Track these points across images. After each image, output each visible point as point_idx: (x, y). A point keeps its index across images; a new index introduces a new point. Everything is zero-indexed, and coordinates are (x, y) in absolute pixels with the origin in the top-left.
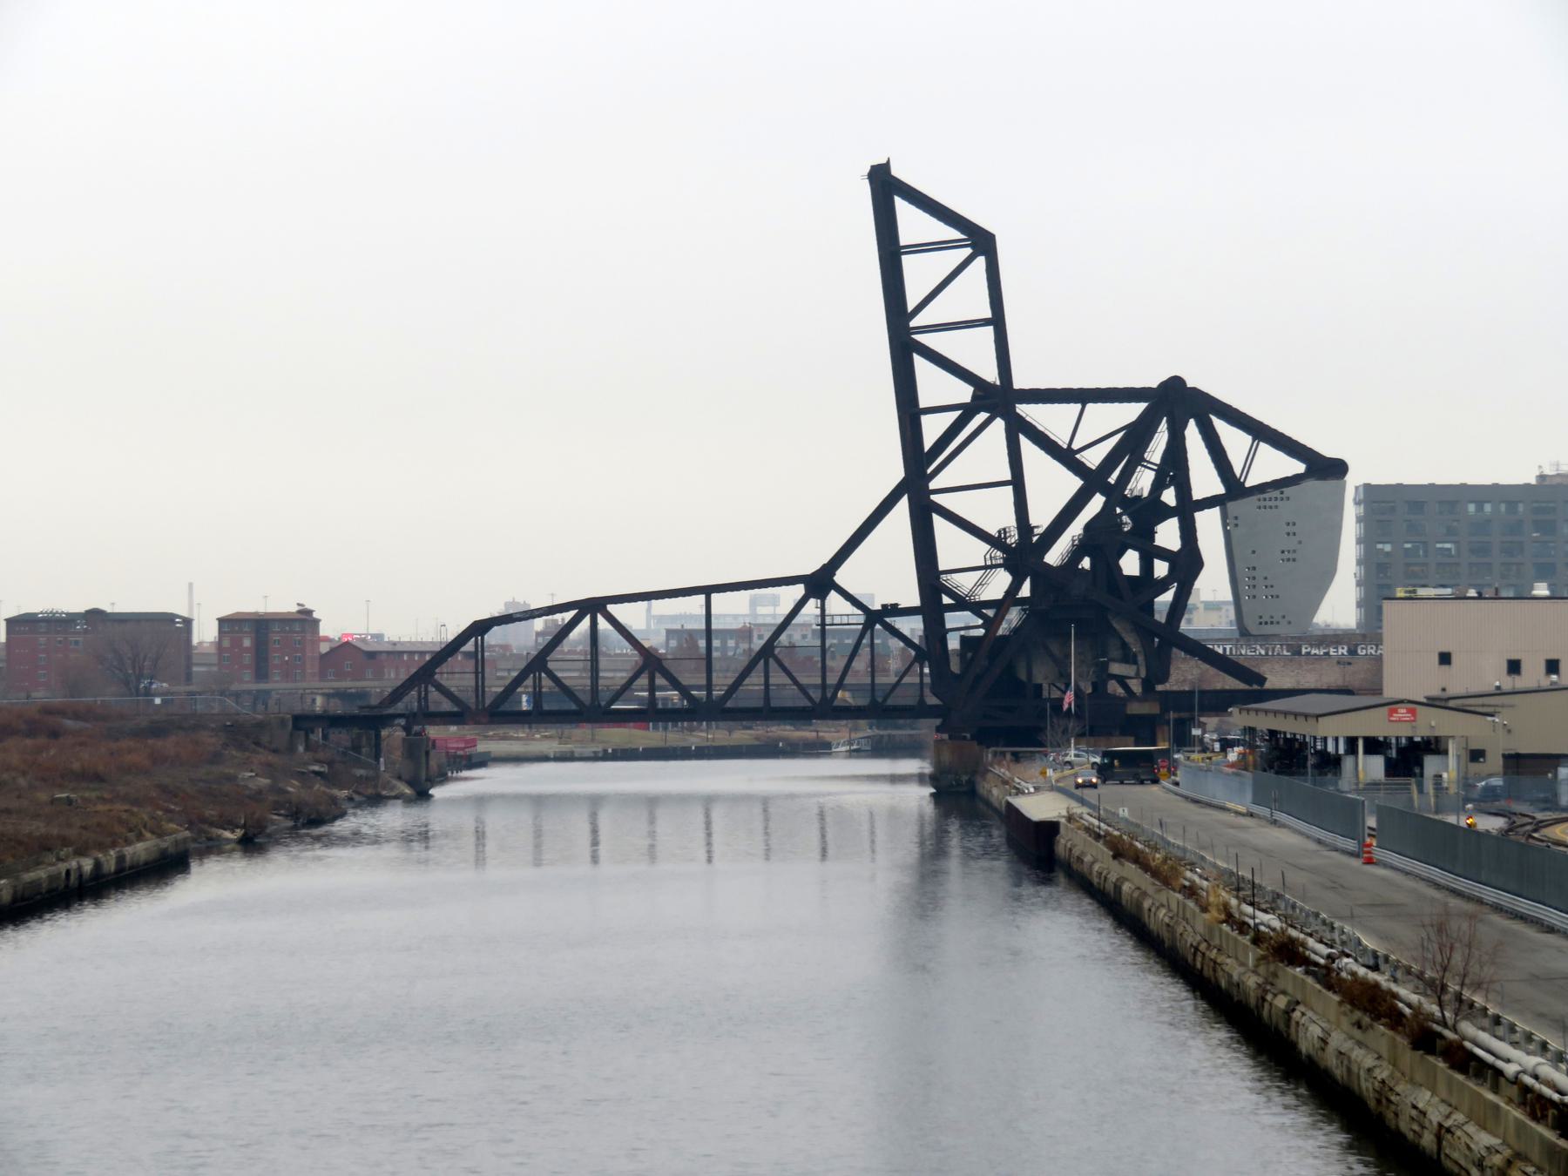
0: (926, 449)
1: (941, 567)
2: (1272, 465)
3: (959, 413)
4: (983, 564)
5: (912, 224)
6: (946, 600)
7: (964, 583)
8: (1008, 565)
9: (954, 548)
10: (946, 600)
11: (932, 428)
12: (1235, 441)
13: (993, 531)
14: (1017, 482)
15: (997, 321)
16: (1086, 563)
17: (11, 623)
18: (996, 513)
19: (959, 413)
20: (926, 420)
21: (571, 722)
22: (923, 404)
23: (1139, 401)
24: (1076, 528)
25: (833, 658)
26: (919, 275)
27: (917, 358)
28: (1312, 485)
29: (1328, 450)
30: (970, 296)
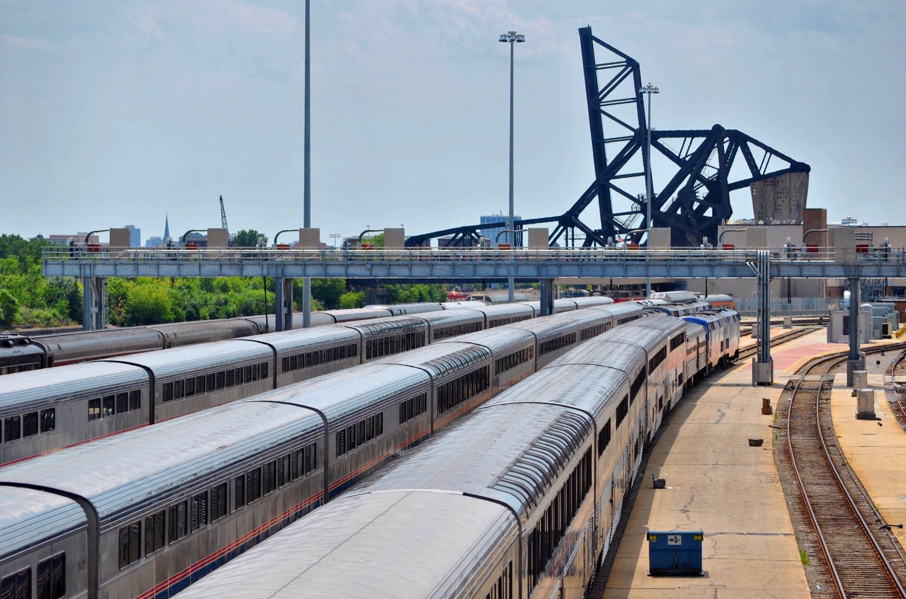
0: (608, 163)
1: (614, 212)
2: (776, 165)
3: (617, 175)
4: (631, 211)
5: (601, 55)
6: (617, 229)
7: (622, 219)
8: (643, 211)
9: (619, 204)
10: (617, 229)
11: (612, 152)
12: (758, 153)
13: (635, 196)
14: (647, 173)
15: (639, 100)
16: (679, 212)
17: (139, 230)
18: (638, 187)
19: (617, 175)
20: (608, 146)
21: (235, 390)
22: (606, 137)
23: (702, 137)
24: (675, 195)
25: (427, 418)
26: (603, 78)
27: (594, 42)
28: (794, 176)
29: (798, 159)
30: (627, 88)
